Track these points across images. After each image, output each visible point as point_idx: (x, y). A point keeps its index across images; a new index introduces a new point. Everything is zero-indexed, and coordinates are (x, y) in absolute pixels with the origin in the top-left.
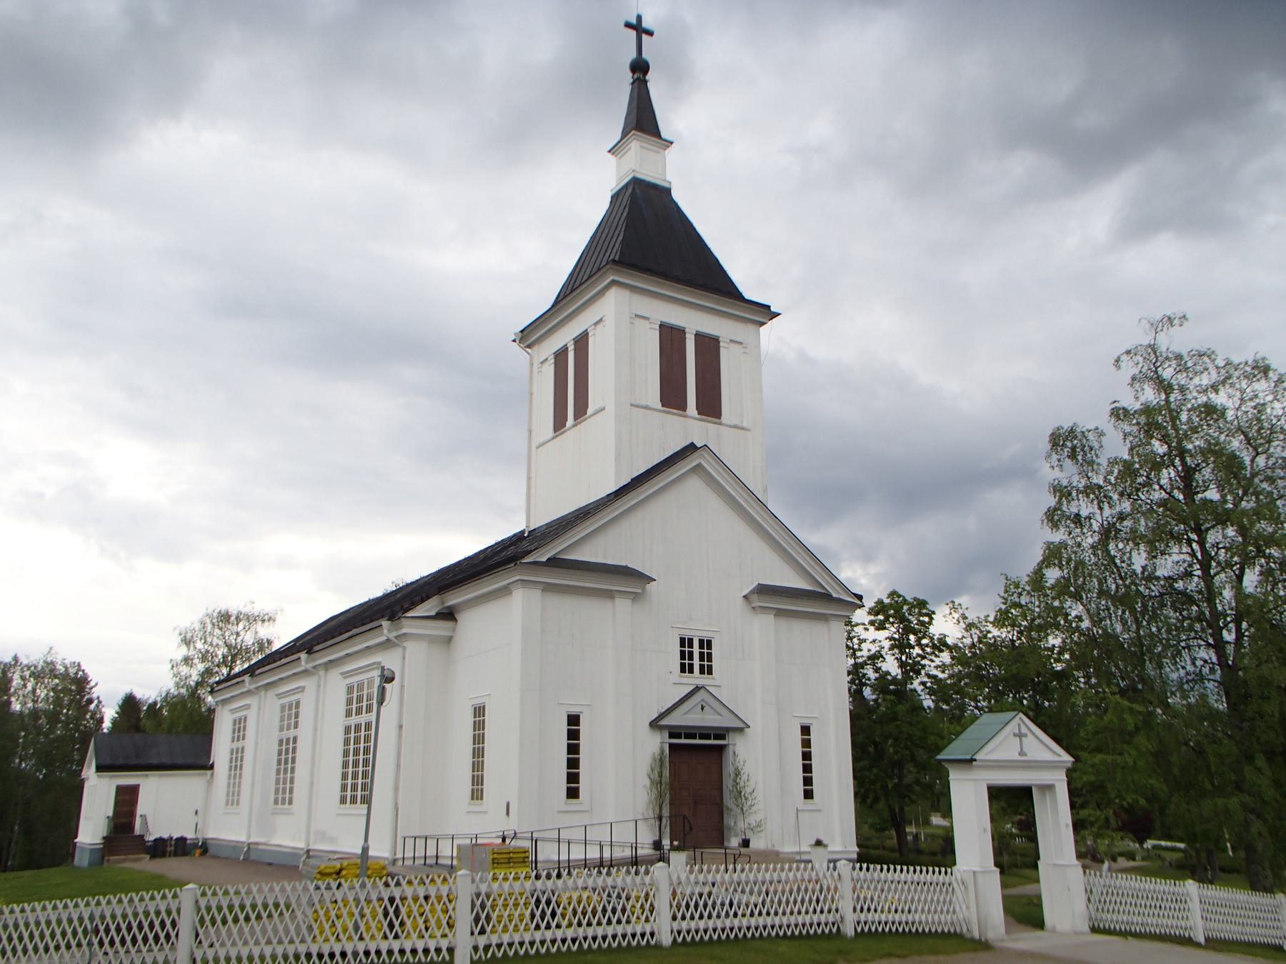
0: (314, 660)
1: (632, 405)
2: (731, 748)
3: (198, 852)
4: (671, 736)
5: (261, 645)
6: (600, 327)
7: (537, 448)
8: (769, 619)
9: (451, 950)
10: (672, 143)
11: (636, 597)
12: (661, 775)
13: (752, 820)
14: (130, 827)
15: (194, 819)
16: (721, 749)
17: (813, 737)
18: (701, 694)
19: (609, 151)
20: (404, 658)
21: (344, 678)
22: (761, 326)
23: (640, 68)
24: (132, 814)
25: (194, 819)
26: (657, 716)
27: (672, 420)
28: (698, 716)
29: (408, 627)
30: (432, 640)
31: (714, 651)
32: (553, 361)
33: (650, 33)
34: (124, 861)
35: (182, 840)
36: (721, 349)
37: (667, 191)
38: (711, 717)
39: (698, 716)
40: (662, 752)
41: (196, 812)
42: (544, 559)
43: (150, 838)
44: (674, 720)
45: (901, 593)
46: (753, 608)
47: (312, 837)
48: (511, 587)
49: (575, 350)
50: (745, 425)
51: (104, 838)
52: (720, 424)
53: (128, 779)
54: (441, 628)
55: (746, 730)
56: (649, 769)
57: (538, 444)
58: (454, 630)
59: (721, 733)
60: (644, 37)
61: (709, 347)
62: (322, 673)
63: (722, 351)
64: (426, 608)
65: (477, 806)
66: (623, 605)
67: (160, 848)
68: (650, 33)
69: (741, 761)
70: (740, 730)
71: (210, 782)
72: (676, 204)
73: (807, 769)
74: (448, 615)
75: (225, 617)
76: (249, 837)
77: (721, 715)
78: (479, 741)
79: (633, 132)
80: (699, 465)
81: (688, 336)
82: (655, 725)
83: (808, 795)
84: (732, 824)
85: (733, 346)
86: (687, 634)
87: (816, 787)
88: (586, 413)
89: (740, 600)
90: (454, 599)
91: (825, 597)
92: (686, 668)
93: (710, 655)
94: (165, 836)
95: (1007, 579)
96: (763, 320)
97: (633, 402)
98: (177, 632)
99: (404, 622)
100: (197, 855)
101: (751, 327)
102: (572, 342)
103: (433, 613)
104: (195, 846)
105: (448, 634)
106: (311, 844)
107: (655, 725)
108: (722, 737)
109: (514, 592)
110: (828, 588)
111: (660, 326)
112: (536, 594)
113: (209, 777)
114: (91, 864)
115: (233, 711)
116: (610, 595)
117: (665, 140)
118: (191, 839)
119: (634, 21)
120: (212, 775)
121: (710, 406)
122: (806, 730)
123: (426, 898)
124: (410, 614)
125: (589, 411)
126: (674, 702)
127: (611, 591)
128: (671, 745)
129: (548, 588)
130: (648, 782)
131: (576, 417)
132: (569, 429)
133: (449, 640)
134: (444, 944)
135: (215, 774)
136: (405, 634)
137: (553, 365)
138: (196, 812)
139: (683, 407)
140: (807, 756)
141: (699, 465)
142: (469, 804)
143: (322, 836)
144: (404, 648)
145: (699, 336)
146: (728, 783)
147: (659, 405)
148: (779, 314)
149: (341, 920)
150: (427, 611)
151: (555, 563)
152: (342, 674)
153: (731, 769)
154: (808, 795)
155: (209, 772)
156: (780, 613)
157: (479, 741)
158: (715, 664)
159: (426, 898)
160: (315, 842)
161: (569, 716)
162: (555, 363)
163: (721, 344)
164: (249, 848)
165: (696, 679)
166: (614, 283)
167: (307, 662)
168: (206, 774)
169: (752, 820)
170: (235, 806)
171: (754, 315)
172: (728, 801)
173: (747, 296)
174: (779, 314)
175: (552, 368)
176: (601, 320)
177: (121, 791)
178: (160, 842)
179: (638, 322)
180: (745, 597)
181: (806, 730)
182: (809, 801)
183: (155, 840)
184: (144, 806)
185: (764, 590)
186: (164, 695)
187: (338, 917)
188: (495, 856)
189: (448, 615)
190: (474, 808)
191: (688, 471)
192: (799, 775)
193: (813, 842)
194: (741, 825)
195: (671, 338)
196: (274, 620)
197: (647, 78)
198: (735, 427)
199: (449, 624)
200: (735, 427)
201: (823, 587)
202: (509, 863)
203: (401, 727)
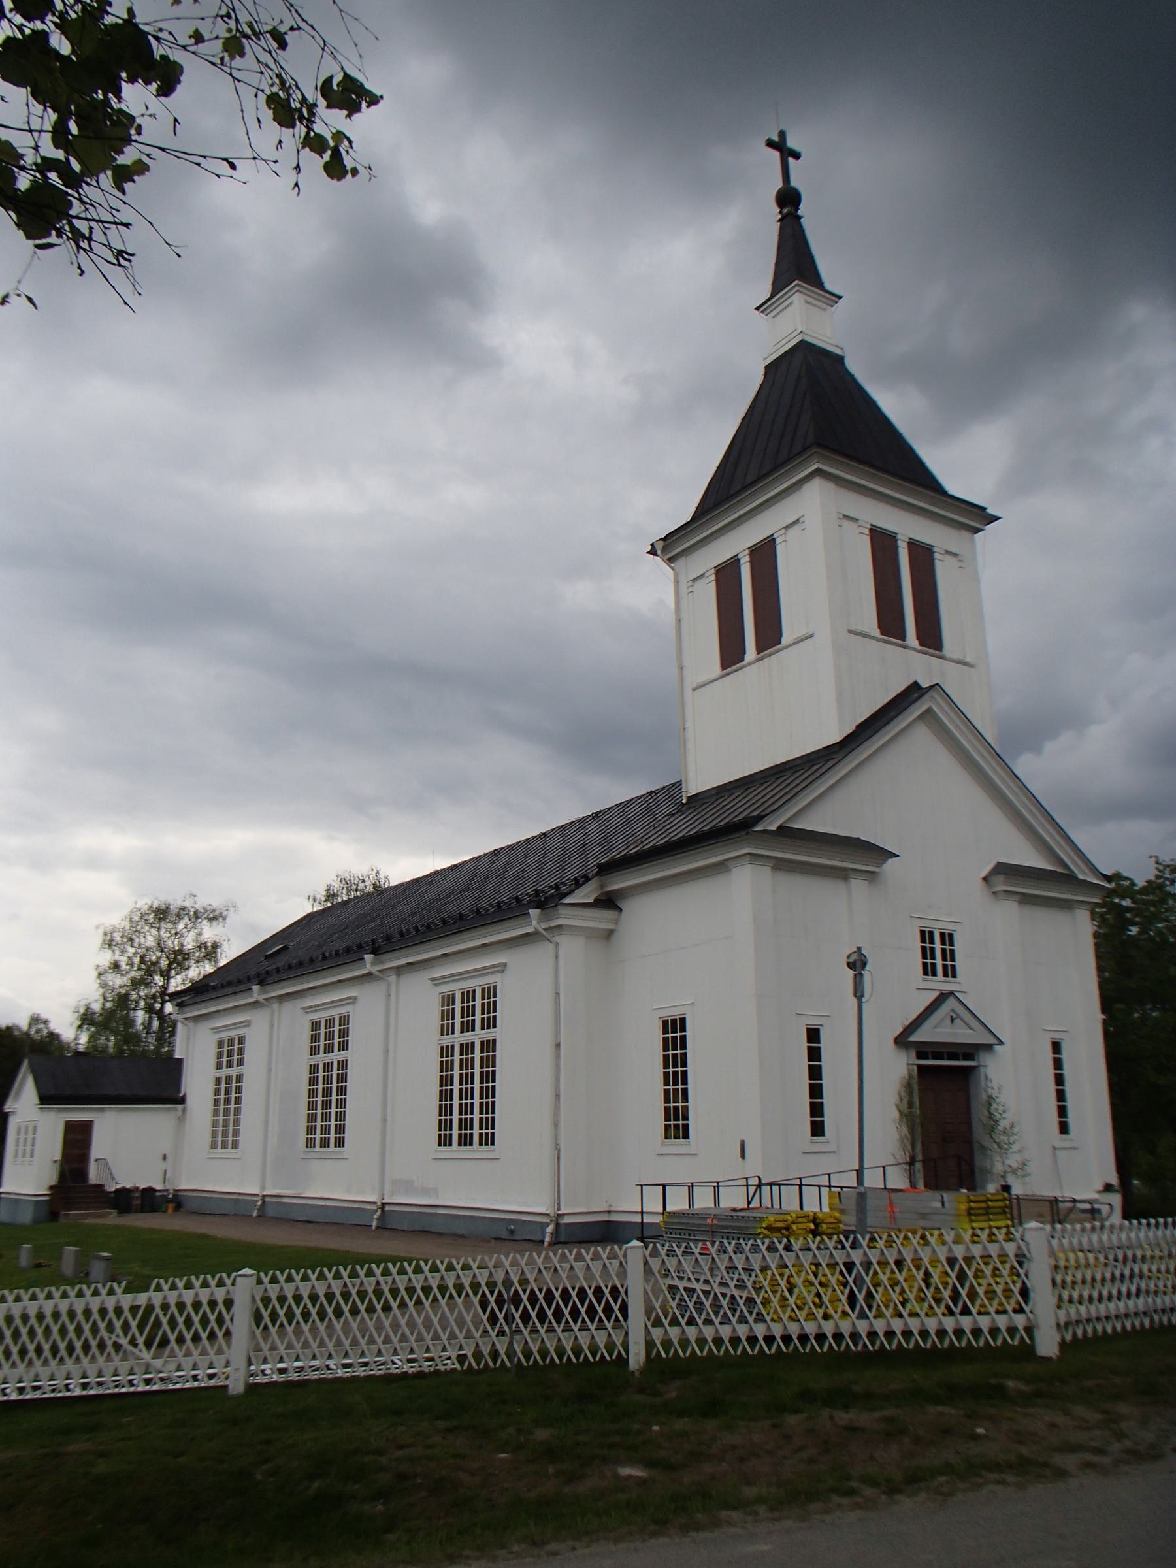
0: (382, 963)
1: (850, 631)
2: (982, 1069)
3: (171, 1206)
4: (921, 1055)
5: (210, 951)
6: (793, 532)
7: (694, 690)
8: (1011, 908)
9: (1029, 1330)
10: (840, 298)
11: (872, 877)
12: (911, 1105)
13: (1013, 1161)
14: (82, 1174)
15: (162, 1166)
16: (967, 1072)
17: (244, 1084)
18: (951, 1003)
19: (757, 309)
20: (557, 957)
21: (436, 985)
22: (976, 533)
23: (788, 199)
24: (84, 1158)
25: (162, 1166)
26: (901, 1030)
27: (891, 651)
28: (948, 1030)
29: (565, 917)
30: (590, 934)
31: (956, 948)
32: (713, 577)
33: (797, 156)
34: (87, 1216)
35: (150, 1191)
36: (937, 562)
37: (840, 360)
38: (962, 1031)
39: (948, 1030)
40: (910, 1076)
41: (165, 1158)
42: (774, 827)
43: (110, 1188)
44: (922, 1035)
45: (1125, 874)
46: (993, 893)
47: (387, 1187)
48: (729, 864)
49: (752, 562)
50: (968, 659)
51: (51, 1188)
52: (943, 658)
53: (79, 1114)
54: (600, 919)
55: (997, 1048)
56: (898, 1097)
57: (695, 685)
58: (617, 922)
59: (970, 1051)
60: (791, 160)
61: (922, 555)
62: (392, 978)
63: (937, 563)
64: (582, 894)
65: (819, 1143)
66: (858, 886)
67: (124, 1200)
68: (797, 156)
69: (995, 1088)
70: (988, 1047)
71: (182, 1119)
72: (852, 376)
73: (1061, 1096)
74: (609, 902)
75: (162, 914)
76: (263, 1188)
77: (971, 1029)
78: (447, 1068)
79: (796, 282)
80: (929, 711)
81: (900, 543)
82: (902, 1041)
83: (1064, 1129)
84: (988, 1166)
85: (949, 558)
86: (928, 925)
87: (1071, 1119)
88: (779, 643)
89: (979, 883)
90: (618, 883)
91: (1067, 879)
92: (928, 970)
93: (924, 956)
94: (128, 1186)
95: (1157, 863)
96: (978, 526)
97: (853, 628)
98: (101, 931)
99: (562, 910)
100: (170, 1211)
101: (965, 534)
102: (747, 552)
103: (591, 900)
104: (165, 1200)
105: (611, 927)
106: (386, 1198)
107: (902, 1041)
108: (969, 1056)
109: (734, 870)
110: (1072, 867)
111: (871, 530)
112: (765, 873)
113: (180, 1113)
114: (36, 1221)
115: (215, 1030)
116: (843, 874)
117: (827, 292)
118: (160, 1191)
119: (776, 138)
120: (184, 1110)
121: (931, 638)
122: (1056, 1047)
123: (899, 1263)
124: (567, 901)
125: (785, 640)
126: (918, 1013)
127: (845, 869)
128: (920, 1067)
129: (780, 865)
130: (896, 1114)
131: (760, 648)
132: (750, 664)
133: (610, 933)
134: (1020, 1320)
135: (188, 1111)
136: (560, 926)
137: (714, 583)
138: (165, 1158)
139: (902, 635)
140: (1059, 1080)
141: (929, 711)
142: (209, 1152)
143: (406, 1186)
144: (557, 945)
145: (913, 545)
146: (979, 1114)
147: (877, 633)
148: (998, 518)
149: (880, 1289)
150: (586, 896)
151: (784, 832)
152: (432, 980)
153: (984, 1097)
154: (1064, 1129)
155: (180, 1107)
156: (1026, 900)
157: (447, 1068)
158: (958, 963)
159: (899, 1263)
160: (392, 1194)
161: (808, 1030)
162: (717, 580)
163: (936, 556)
164: (264, 1202)
165: (941, 983)
166: (818, 472)
167: (373, 964)
168: (176, 1109)
169: (1013, 1161)
170: (27, 1158)
171: (963, 517)
172: (979, 1133)
173: (953, 487)
174: (998, 518)
175: (712, 587)
176: (797, 521)
177: (70, 1127)
178: (123, 1193)
179: (846, 523)
180: (985, 879)
181: (1056, 1047)
182: (1064, 1136)
183: (117, 1191)
184: (98, 1149)
185: (1003, 870)
186: (82, 1010)
187: (876, 1285)
188: (972, 1204)
189: (609, 902)
190: (666, 1150)
191: (915, 720)
192: (1053, 1103)
193: (1101, 1188)
194: (999, 1168)
195: (883, 543)
196: (225, 918)
197: (800, 213)
198: (959, 662)
199: (609, 914)
200: (959, 662)
201: (1069, 869)
202: (987, 1214)
203: (558, 1045)
